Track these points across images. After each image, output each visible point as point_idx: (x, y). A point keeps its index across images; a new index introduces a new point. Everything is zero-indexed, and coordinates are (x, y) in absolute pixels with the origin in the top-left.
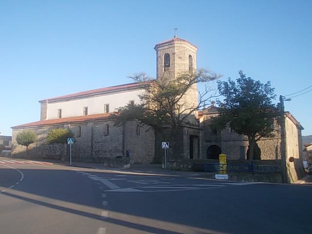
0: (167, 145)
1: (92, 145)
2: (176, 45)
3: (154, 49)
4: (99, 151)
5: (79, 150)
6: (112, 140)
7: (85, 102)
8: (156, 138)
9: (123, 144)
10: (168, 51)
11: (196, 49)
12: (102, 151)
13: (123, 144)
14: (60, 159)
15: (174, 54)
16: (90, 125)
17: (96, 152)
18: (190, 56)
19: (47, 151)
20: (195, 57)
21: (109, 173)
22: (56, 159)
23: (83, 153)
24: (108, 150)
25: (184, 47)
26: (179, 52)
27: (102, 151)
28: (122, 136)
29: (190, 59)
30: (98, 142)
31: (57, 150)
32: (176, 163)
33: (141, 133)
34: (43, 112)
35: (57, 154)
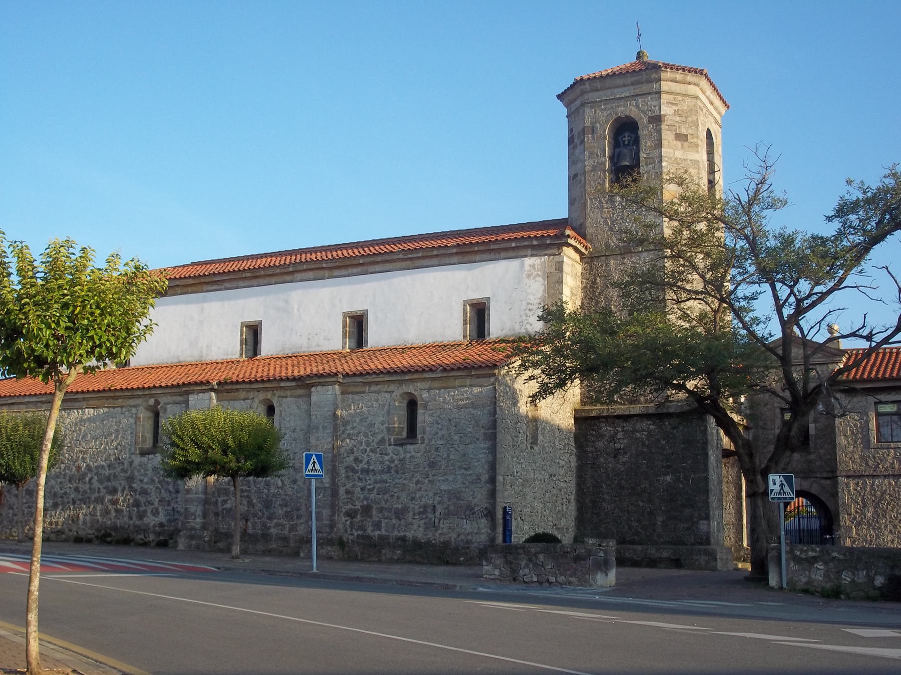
0: (787, 489)
1: (334, 483)
2: (665, 86)
4: (367, 510)
5: (268, 504)
6: (432, 465)
7: (249, 304)
8: (579, 458)
10: (631, 110)
11: (723, 110)
12: (381, 510)
13: (493, 480)
14: (163, 544)
15: (657, 120)
16: (325, 396)
17: (351, 514)
18: (709, 132)
20: (719, 136)
21: (829, 651)
22: (145, 544)
23: (288, 515)
25: (697, 97)
26: (676, 113)
27: (381, 510)
28: (484, 445)
29: (616, 143)
30: (366, 471)
31: (150, 503)
32: (826, 563)
33: (540, 438)
35: (151, 520)
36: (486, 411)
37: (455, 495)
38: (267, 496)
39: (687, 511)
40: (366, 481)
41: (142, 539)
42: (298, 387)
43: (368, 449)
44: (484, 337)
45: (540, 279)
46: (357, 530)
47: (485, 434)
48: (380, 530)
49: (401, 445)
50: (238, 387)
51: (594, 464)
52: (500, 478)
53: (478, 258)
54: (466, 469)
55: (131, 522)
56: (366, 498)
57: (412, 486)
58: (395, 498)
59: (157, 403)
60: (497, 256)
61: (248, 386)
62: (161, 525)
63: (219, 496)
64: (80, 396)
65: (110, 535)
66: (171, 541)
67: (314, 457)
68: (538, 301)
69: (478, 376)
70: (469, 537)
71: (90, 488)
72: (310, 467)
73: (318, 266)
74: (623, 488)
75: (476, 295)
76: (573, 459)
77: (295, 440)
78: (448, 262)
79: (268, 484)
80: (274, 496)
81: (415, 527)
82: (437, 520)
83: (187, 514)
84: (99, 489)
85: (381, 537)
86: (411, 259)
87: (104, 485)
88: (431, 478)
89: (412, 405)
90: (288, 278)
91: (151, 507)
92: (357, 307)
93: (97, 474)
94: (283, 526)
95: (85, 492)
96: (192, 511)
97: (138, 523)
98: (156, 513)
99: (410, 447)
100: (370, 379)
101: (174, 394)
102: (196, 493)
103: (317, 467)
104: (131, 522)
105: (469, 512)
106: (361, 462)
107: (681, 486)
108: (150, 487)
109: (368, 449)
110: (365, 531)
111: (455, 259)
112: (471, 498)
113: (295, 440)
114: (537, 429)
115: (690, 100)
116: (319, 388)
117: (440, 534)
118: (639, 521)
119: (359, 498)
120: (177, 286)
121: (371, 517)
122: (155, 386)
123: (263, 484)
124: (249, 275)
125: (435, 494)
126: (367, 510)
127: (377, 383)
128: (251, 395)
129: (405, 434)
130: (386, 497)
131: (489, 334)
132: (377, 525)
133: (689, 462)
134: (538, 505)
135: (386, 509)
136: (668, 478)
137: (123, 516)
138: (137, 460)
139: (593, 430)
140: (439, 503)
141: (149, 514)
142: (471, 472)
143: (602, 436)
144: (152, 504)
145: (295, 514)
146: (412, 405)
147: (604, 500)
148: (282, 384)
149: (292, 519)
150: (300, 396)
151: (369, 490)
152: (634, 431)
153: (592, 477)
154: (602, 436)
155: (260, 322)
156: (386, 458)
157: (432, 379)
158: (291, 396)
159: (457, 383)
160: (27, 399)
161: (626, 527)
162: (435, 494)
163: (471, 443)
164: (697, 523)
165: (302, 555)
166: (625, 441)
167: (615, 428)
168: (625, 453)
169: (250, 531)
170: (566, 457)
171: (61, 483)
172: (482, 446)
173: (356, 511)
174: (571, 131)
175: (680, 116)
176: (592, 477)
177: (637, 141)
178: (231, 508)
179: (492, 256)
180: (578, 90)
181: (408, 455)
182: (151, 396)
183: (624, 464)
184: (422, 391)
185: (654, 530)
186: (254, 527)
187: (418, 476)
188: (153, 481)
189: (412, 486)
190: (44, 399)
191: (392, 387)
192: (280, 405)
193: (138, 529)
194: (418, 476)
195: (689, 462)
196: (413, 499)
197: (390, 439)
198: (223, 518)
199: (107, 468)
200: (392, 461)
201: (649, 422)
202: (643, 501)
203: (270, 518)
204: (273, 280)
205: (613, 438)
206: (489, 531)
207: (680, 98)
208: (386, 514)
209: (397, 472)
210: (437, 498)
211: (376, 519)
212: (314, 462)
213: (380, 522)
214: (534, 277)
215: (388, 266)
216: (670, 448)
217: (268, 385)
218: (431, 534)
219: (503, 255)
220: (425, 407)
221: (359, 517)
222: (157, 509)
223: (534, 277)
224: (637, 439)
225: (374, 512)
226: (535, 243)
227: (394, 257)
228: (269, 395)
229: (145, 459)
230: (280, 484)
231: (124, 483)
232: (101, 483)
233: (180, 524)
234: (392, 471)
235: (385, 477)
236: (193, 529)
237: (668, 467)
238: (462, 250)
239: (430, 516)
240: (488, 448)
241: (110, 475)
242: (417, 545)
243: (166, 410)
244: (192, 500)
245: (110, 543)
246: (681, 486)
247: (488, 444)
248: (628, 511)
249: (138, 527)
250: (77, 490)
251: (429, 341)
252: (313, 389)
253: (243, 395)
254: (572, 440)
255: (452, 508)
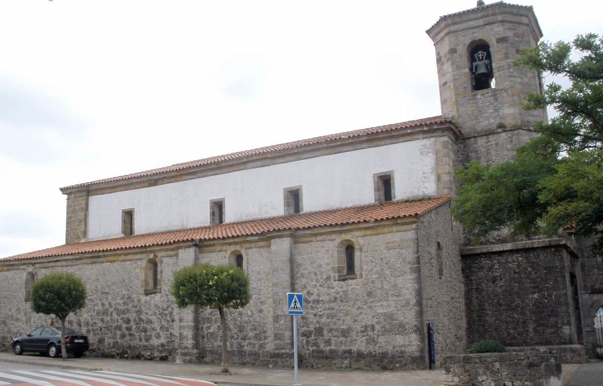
3: (428, 32)
5: (241, 329)
6: (370, 294)
8: (466, 285)
9: (419, 303)
12: (331, 330)
14: (164, 359)
19: (119, 333)
22: (151, 359)
23: (257, 337)
24: (358, 327)
30: (317, 302)
31: (154, 329)
34: (77, 219)
35: (155, 342)
36: (410, 251)
37: (390, 317)
38: (241, 323)
39: (553, 320)
40: (318, 309)
41: (149, 356)
42: (261, 240)
43: (318, 285)
44: (390, 199)
45: (431, 155)
46: (312, 346)
47: (411, 268)
48: (330, 346)
49: (344, 280)
50: (215, 242)
51: (478, 288)
52: (424, 302)
53: (382, 143)
54: (397, 296)
55: (141, 343)
56: (318, 322)
57: (355, 311)
58: (341, 321)
59: (156, 256)
60: (397, 141)
61: (222, 241)
62: (163, 345)
63: (204, 324)
64: (101, 254)
65: (127, 353)
66: (170, 357)
67: (295, 297)
68: (431, 171)
69: (403, 224)
70: (403, 348)
71: (111, 320)
72: (292, 305)
73: (264, 156)
74: (501, 305)
75: (383, 170)
76: (462, 285)
77: (260, 280)
78: (360, 147)
79: (240, 314)
80: (246, 322)
81: (359, 342)
82: (376, 337)
83: (181, 337)
84: (117, 319)
85: (331, 351)
86: (332, 147)
87: (121, 317)
88: (369, 304)
89: (349, 249)
90: (242, 167)
91: (155, 332)
92: (292, 184)
93: (115, 309)
94: (254, 345)
95: (108, 322)
96: (185, 335)
97: (145, 343)
98: (158, 336)
99: (350, 281)
100: (316, 231)
101: (166, 250)
102: (187, 322)
103: (298, 305)
104: (141, 343)
105: (401, 328)
106: (312, 294)
107: (546, 301)
108: (153, 318)
109: (318, 285)
110: (318, 346)
111: (365, 145)
112: (402, 318)
113: (260, 280)
114: (442, 264)
115: (523, 26)
116: (277, 240)
117: (379, 347)
118: (515, 329)
119: (312, 322)
120: (165, 177)
121: (322, 336)
122: (153, 245)
123: (237, 314)
124: (214, 166)
125: (373, 317)
126: (319, 331)
127: (322, 234)
128: (224, 248)
129: (345, 272)
130: (334, 320)
131: (395, 197)
132: (328, 342)
133: (551, 283)
134: (446, 321)
135: (334, 330)
136: (536, 296)
137: (136, 339)
138: (143, 298)
139: (476, 263)
140: (377, 323)
141: (153, 337)
142: (402, 298)
143: (482, 268)
144: (156, 330)
145: (263, 335)
146: (349, 249)
147: (487, 314)
148: (248, 239)
149: (260, 339)
150: (261, 247)
151: (320, 316)
152: (507, 262)
153: (477, 298)
154: (482, 268)
155: (224, 199)
156: (333, 291)
157: (366, 229)
158: (255, 247)
159: (386, 230)
160: (67, 257)
161: (506, 334)
162: (373, 317)
163: (399, 276)
164: (561, 328)
165: (270, 366)
166: (501, 270)
167: (492, 261)
168: (501, 279)
169: (229, 349)
170: (459, 284)
171: (91, 316)
172: (409, 277)
173: (310, 333)
174: (438, 54)
175: (518, 37)
176: (477, 298)
177: (489, 56)
178: (213, 333)
179: (393, 141)
180: (443, 25)
181: (350, 288)
182: (151, 252)
183: (501, 287)
184: (356, 237)
185: (527, 335)
186: (232, 346)
187: (359, 304)
188: (155, 313)
189: (355, 311)
190: (78, 257)
191: (334, 236)
192: (247, 254)
193: (146, 348)
194: (359, 304)
195: (551, 283)
196: (355, 321)
197: (334, 276)
198: (208, 339)
199: (122, 305)
200: (338, 293)
201: (518, 255)
202: (517, 314)
203: (244, 339)
204: (232, 169)
205: (491, 268)
206: (419, 343)
207: (517, 25)
208: (335, 334)
209: (342, 301)
210: (375, 320)
211: (326, 337)
212: (295, 301)
213: (330, 340)
214: (426, 154)
215: (315, 154)
216: (536, 273)
217: (237, 240)
218: (371, 347)
219: (401, 139)
220: (361, 250)
221: (313, 337)
222: (159, 334)
223: (426, 154)
224: (510, 268)
225: (325, 332)
226: (425, 129)
227: (320, 146)
228: (238, 248)
229: (148, 298)
230: (249, 313)
231: (134, 315)
232: (119, 315)
233: (176, 344)
234: (338, 300)
235: (332, 305)
236: (186, 348)
237: (536, 287)
238: (371, 138)
239: (370, 333)
240: (415, 279)
241: (125, 310)
242: (360, 356)
243: (162, 262)
244: (184, 327)
245: (127, 358)
246: (546, 301)
247: (415, 275)
248: (506, 322)
249: (146, 346)
250: (102, 320)
251: (349, 205)
252: (272, 241)
253: (219, 248)
254: (461, 271)
255: (388, 327)
